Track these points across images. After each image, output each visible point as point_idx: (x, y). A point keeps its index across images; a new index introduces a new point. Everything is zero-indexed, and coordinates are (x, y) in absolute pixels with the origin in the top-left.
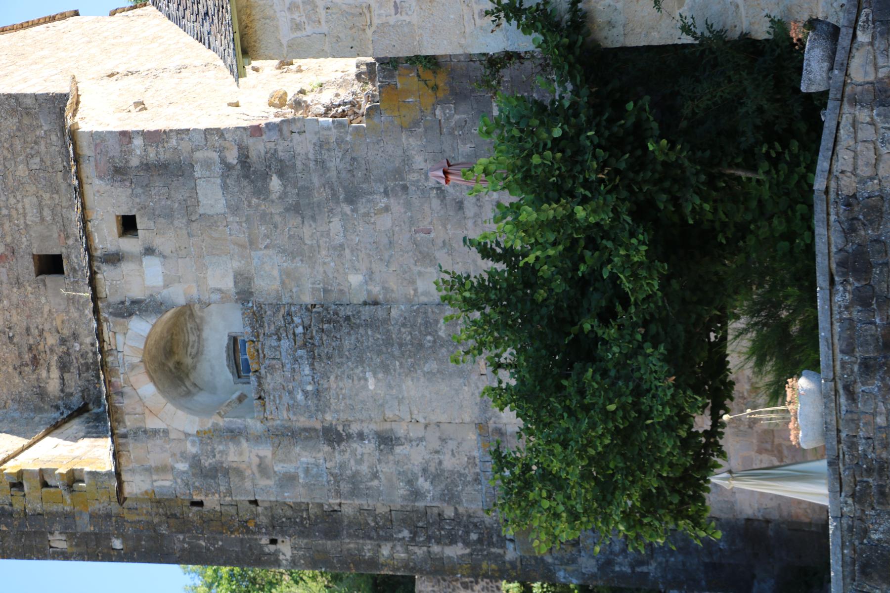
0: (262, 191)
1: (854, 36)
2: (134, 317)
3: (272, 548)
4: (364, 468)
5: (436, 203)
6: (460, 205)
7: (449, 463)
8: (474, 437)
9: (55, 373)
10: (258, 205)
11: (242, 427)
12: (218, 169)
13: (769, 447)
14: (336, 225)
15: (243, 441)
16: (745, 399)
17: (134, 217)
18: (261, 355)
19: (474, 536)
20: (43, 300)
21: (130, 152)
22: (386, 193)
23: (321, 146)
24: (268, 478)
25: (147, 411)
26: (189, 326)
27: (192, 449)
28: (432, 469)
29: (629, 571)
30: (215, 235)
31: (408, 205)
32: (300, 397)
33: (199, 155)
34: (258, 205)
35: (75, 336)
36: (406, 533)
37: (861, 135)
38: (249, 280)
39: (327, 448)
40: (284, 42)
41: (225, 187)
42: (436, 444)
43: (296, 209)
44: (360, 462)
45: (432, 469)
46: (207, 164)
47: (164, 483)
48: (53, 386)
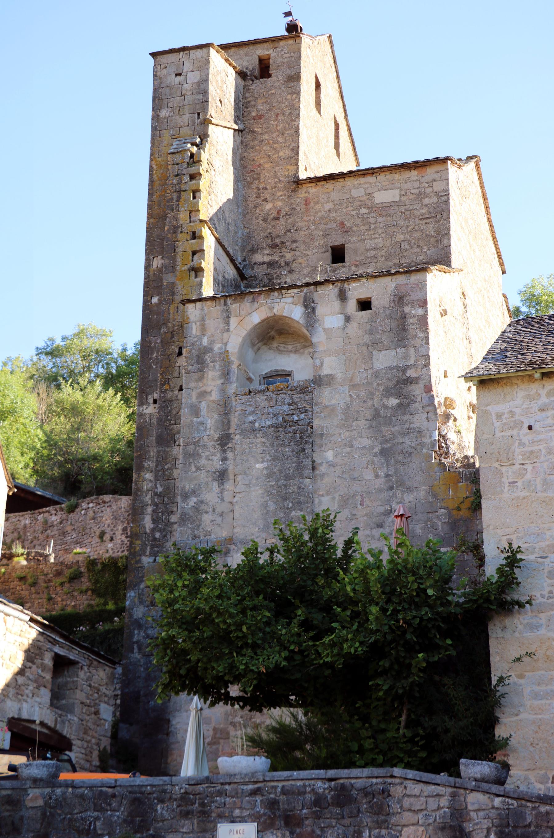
0: (388, 393)
1: (498, 796)
2: (304, 309)
3: (151, 401)
4: (203, 461)
5: (381, 509)
6: (380, 525)
7: (207, 518)
8: (224, 535)
9: (266, 259)
10: (379, 390)
11: (231, 380)
12: (403, 363)
13: (218, 735)
14: (366, 442)
15: (222, 381)
16: (231, 723)
17: (370, 309)
18: (278, 393)
19: (157, 535)
20: (315, 251)
21: (413, 307)
22: (388, 476)
23: (419, 432)
24: (197, 398)
25: (241, 318)
26: (298, 345)
27: (217, 348)
28: (203, 507)
29: (135, 640)
30: (358, 363)
31: (380, 491)
32: (251, 418)
33: (412, 351)
34: (379, 390)
35: (291, 271)
36: (160, 489)
37: (431, 800)
38: (329, 384)
39: (216, 436)
40: (489, 408)
41: (391, 368)
42: (219, 510)
43: (377, 415)
44: (208, 458)
45: (203, 507)
46: (406, 357)
47: (194, 330)
48: (258, 258)
